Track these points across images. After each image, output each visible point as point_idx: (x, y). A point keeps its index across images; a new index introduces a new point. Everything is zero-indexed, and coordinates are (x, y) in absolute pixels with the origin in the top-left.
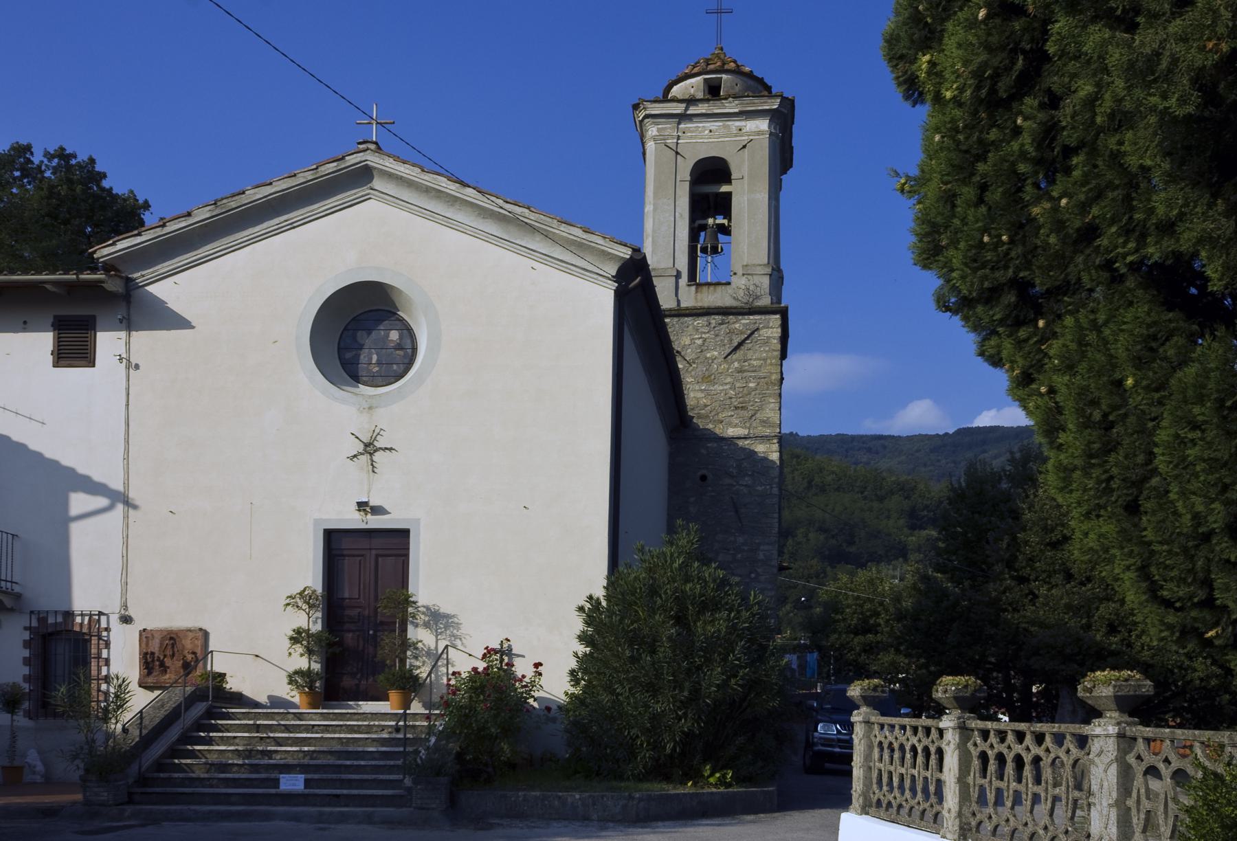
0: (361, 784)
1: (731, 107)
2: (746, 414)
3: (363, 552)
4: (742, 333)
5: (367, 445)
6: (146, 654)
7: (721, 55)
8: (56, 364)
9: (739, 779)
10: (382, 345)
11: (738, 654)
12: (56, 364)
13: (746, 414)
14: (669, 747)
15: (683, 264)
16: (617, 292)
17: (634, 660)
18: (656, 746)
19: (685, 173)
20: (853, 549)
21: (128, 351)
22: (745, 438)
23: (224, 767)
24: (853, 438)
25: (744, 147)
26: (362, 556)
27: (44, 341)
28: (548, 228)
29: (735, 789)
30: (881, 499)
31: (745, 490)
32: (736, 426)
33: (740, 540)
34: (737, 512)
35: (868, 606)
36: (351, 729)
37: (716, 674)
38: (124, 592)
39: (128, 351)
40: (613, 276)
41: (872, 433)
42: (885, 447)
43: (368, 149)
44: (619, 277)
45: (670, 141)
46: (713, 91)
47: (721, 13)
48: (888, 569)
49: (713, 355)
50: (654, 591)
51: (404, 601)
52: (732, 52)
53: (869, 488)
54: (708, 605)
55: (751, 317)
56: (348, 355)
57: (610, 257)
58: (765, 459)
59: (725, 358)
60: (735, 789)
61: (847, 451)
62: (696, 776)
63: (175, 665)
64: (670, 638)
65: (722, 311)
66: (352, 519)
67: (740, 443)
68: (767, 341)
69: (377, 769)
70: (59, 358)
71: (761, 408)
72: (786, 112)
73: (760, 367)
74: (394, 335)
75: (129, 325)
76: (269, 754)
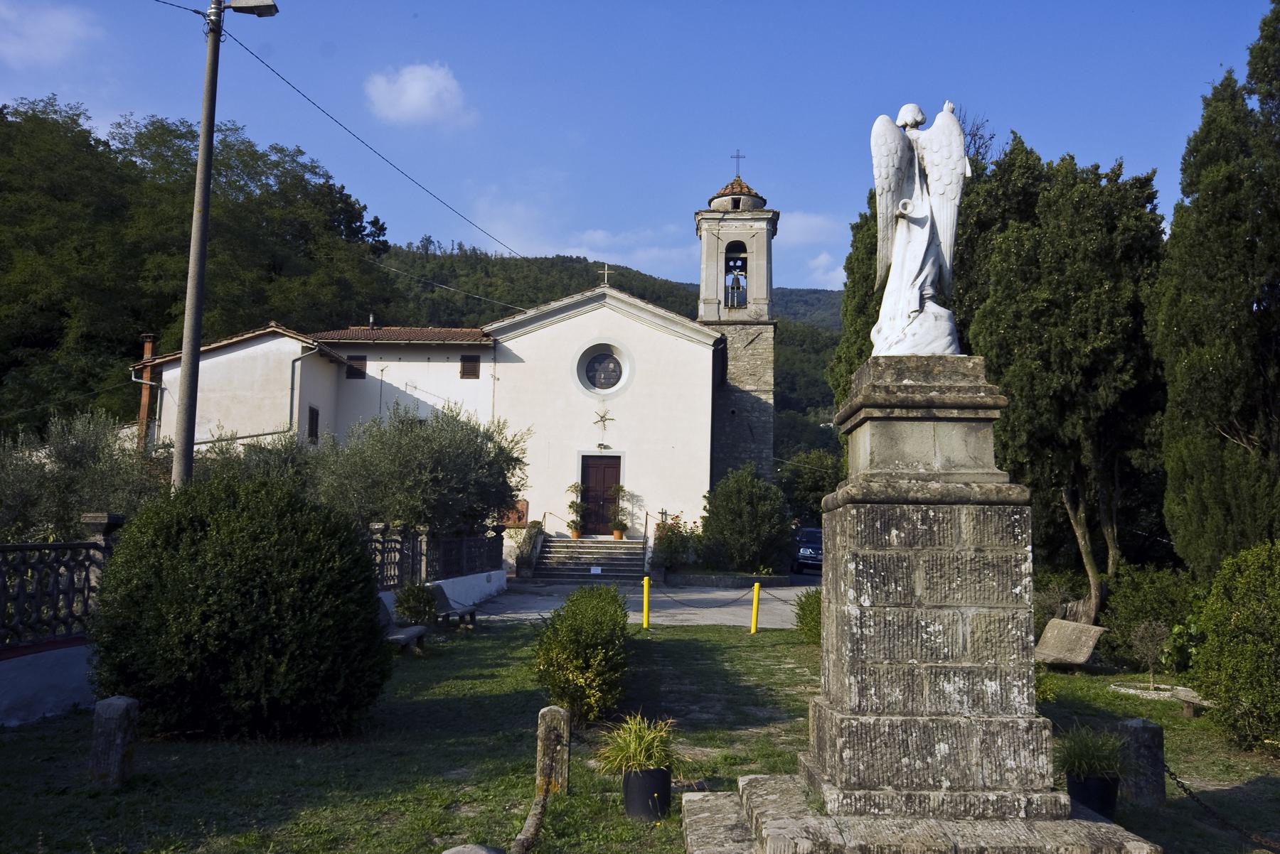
0: (624, 571)
1: (747, 215)
2: (756, 378)
4: (753, 334)
7: (738, 182)
8: (462, 378)
9: (775, 572)
10: (606, 370)
11: (775, 520)
12: (462, 378)
13: (756, 378)
14: (747, 557)
16: (714, 351)
17: (733, 521)
18: (742, 557)
19: (723, 249)
20: (794, 395)
21: (495, 372)
22: (755, 391)
23: (564, 564)
24: (792, 292)
27: (456, 367)
29: (773, 576)
30: (817, 352)
31: (755, 419)
32: (750, 384)
33: (753, 446)
34: (751, 431)
35: (818, 474)
36: (607, 548)
37: (766, 528)
39: (495, 372)
41: (809, 288)
42: (819, 300)
46: (736, 204)
48: (824, 414)
50: (739, 492)
51: (620, 489)
52: (746, 180)
53: (807, 342)
54: (763, 498)
56: (591, 374)
57: (711, 336)
58: (766, 402)
60: (773, 576)
61: (787, 303)
62: (758, 571)
64: (748, 513)
66: (596, 452)
67: (753, 394)
68: (766, 340)
69: (627, 565)
71: (764, 375)
74: (612, 366)
75: (495, 360)
76: (579, 558)
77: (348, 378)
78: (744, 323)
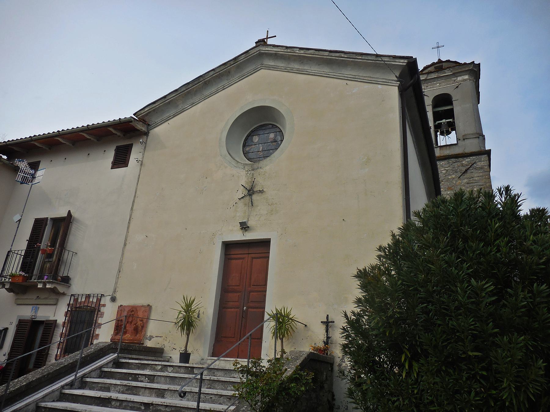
4: (467, 165)
5: (249, 191)
25: (457, 87)
26: (243, 258)
38: (116, 283)
44: (400, 78)
47: (439, 47)
49: (453, 177)
55: (471, 158)
57: (397, 86)
59: (459, 178)
63: (130, 328)
70: (114, 165)
72: (476, 70)
73: (479, 180)
74: (272, 136)
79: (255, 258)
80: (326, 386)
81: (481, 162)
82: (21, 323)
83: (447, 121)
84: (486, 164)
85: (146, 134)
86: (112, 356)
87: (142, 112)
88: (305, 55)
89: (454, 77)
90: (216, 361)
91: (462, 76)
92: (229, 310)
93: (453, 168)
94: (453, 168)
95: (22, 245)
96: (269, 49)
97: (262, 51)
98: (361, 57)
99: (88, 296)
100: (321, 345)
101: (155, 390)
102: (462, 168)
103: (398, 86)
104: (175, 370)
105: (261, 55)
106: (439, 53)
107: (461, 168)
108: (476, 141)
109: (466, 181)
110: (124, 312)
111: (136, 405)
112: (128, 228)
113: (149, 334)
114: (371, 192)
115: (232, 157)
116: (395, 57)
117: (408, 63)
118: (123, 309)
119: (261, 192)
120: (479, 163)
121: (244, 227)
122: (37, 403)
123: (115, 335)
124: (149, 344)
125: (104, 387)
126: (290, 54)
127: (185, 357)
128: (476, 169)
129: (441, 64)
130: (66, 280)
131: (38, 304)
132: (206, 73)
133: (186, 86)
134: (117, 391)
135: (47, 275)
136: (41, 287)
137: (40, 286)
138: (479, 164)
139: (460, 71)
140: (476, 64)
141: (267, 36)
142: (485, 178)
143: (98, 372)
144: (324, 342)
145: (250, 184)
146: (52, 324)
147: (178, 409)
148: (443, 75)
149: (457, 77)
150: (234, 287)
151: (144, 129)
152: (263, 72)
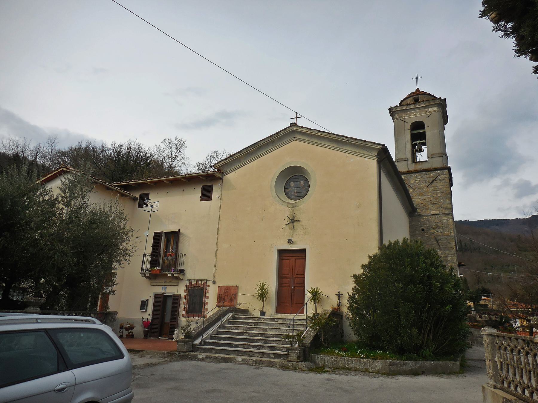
1: (422, 105)
3: (290, 258)
4: (433, 177)
6: (219, 295)
15: (409, 156)
19: (408, 126)
25: (428, 116)
26: (290, 259)
27: (197, 193)
28: (352, 142)
32: (434, 210)
38: (214, 273)
40: (375, 155)
43: (293, 125)
44: (378, 155)
45: (402, 118)
55: (437, 172)
65: (425, 170)
74: (302, 183)
77: (139, 208)
78: (426, 170)
79: (296, 259)
80: (339, 326)
81: (444, 175)
82: (157, 297)
83: (421, 141)
84: (446, 177)
85: (222, 179)
86: (230, 315)
87: (218, 164)
88: (322, 135)
89: (427, 108)
90: (296, 316)
91: (433, 108)
92: (284, 288)
93: (424, 179)
94: (424, 179)
95: (149, 251)
96: (299, 129)
97: (294, 130)
98: (355, 141)
99: (198, 281)
100: (336, 306)
101: (261, 329)
102: (430, 179)
103: (377, 160)
104: (265, 320)
105: (294, 132)
106: (417, 83)
107: (429, 179)
108: (440, 159)
109: (432, 189)
110: (222, 290)
111: (256, 334)
112: (217, 240)
113: (239, 302)
114: (361, 224)
115: (280, 198)
116: (375, 143)
117: (382, 148)
118: (221, 288)
119: (299, 221)
120: (442, 176)
121: (290, 242)
122: (211, 335)
123: (219, 303)
124: (239, 307)
125: (235, 328)
126: (312, 133)
127: (263, 313)
128: (440, 180)
129: (418, 96)
130: (182, 271)
131: (165, 285)
132: (259, 142)
133: (246, 149)
134: (242, 329)
135: (173, 269)
136: (170, 276)
137: (170, 275)
138: (442, 177)
139: (430, 104)
140: (443, 99)
141: (296, 116)
142: (446, 187)
143: (227, 321)
144: (337, 305)
145: (292, 216)
146: (178, 297)
147: (277, 335)
148: (418, 107)
149: (429, 108)
150: (285, 275)
151: (220, 176)
152: (295, 143)
